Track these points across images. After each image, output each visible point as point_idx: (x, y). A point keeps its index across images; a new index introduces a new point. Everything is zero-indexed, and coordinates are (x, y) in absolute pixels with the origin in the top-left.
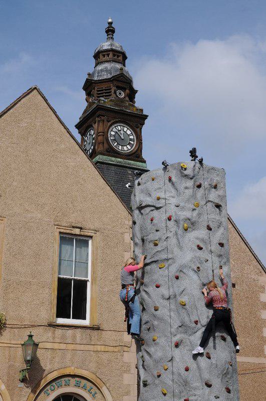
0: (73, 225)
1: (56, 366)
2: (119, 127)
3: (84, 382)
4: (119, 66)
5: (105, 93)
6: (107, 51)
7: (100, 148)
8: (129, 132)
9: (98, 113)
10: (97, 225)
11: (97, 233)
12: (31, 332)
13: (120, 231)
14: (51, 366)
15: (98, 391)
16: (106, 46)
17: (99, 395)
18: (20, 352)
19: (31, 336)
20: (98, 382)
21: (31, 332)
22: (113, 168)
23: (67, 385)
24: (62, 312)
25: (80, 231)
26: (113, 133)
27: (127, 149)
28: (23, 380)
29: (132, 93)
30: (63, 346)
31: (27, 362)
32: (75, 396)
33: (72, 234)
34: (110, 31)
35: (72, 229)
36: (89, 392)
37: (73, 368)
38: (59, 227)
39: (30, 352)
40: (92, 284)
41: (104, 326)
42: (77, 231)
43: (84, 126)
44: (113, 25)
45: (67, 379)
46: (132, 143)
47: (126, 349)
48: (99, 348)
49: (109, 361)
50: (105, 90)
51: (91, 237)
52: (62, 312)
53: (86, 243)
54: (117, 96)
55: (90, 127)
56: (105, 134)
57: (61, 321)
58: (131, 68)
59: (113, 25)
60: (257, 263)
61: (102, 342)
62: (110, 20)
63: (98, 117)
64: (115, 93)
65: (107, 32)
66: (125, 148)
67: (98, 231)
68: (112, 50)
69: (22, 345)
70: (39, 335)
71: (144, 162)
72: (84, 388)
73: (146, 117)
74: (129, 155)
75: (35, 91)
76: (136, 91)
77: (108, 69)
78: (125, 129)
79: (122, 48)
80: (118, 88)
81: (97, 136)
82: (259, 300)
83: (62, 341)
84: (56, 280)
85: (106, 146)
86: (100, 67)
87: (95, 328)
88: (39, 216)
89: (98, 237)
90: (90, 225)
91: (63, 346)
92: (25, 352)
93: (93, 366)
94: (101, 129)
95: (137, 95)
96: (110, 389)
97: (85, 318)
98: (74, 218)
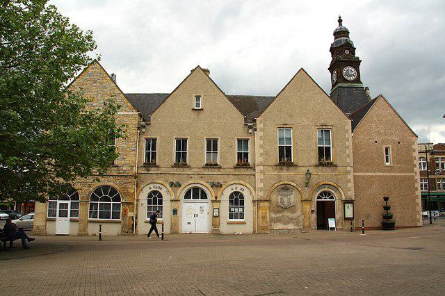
17: (338, 192)
34: (340, 21)
89: (334, 129)
98: (322, 122)
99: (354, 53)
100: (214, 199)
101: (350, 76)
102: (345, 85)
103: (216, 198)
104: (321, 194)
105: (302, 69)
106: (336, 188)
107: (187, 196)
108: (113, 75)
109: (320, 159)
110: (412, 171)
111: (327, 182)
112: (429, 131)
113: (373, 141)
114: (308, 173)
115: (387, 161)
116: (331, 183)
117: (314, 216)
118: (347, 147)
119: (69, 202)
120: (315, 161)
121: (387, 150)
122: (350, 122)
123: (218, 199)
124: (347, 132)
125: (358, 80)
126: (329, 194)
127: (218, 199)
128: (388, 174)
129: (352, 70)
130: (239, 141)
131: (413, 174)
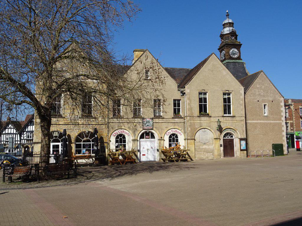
4: (231, 28)
6: (227, 23)
7: (227, 57)
8: (236, 51)
9: (226, 46)
10: (232, 89)
14: (223, 126)
17: (236, 132)
22: (232, 63)
24: (225, 113)
26: (231, 52)
27: (236, 56)
28: (218, 130)
31: (218, 126)
39: (219, 123)
42: (227, 92)
43: (221, 49)
51: (231, 93)
52: (225, 113)
53: (230, 94)
55: (223, 50)
56: (228, 52)
57: (225, 115)
62: (227, 11)
63: (226, 47)
64: (231, 38)
70: (221, 119)
74: (237, 58)
80: (232, 36)
81: (226, 53)
84: (223, 105)
85: (229, 56)
87: (233, 117)
89: (233, 93)
90: (231, 89)
92: (218, 123)
93: (234, 126)
94: (227, 51)
98: (226, 88)
100: (160, 139)
101: (234, 54)
102: (232, 61)
103: (161, 138)
107: (142, 137)
109: (200, 112)
110: (280, 120)
113: (256, 100)
114: (219, 121)
115: (265, 113)
117: (222, 148)
119: (60, 144)
120: (221, 113)
121: (265, 106)
122: (243, 88)
123: (163, 139)
125: (239, 58)
127: (163, 139)
128: (266, 122)
130: (175, 100)
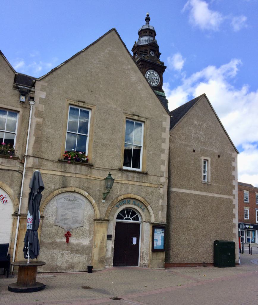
0: (134, 114)
1: (123, 193)
2: (151, 72)
3: (138, 202)
4: (152, 38)
5: (144, 53)
10: (147, 115)
11: (147, 120)
12: (110, 172)
13: (160, 120)
15: (145, 208)
16: (146, 27)
17: (146, 210)
18: (103, 183)
19: (110, 175)
20: (146, 203)
21: (110, 172)
23: (129, 203)
25: (138, 118)
29: (158, 54)
30: (127, 182)
32: (129, 208)
33: (133, 119)
34: (148, 19)
35: (133, 116)
36: (141, 208)
37: (132, 194)
38: (126, 114)
40: (144, 148)
41: (150, 173)
42: (136, 118)
44: (149, 16)
45: (128, 200)
46: (158, 81)
47: (161, 186)
48: (146, 185)
49: (152, 192)
50: (144, 51)
51: (144, 122)
54: (151, 55)
57: (125, 168)
58: (158, 39)
59: (149, 16)
60: (232, 145)
61: (148, 181)
64: (150, 53)
65: (146, 20)
66: (154, 84)
67: (148, 119)
68: (149, 29)
69: (105, 179)
71: (163, 92)
72: (138, 205)
73: (166, 67)
74: (156, 88)
75: (114, 32)
76: (160, 54)
77: (145, 40)
78: (154, 73)
79: (154, 28)
82: (232, 165)
83: (127, 179)
86: (142, 39)
87: (145, 173)
88: (115, 106)
90: (144, 114)
91: (127, 182)
93: (143, 194)
95: (160, 56)
96: (152, 207)
97: (139, 168)
98: (134, 110)
99: (158, 57)
104: (122, 212)
105: (114, 30)
106: (144, 205)
108: (99, 230)
110: (230, 193)
111: (132, 195)
112: (108, 177)
114: (110, 179)
116: (139, 197)
118: (162, 151)
124: (164, 130)
126: (134, 213)
129: (156, 76)
131: (232, 197)
